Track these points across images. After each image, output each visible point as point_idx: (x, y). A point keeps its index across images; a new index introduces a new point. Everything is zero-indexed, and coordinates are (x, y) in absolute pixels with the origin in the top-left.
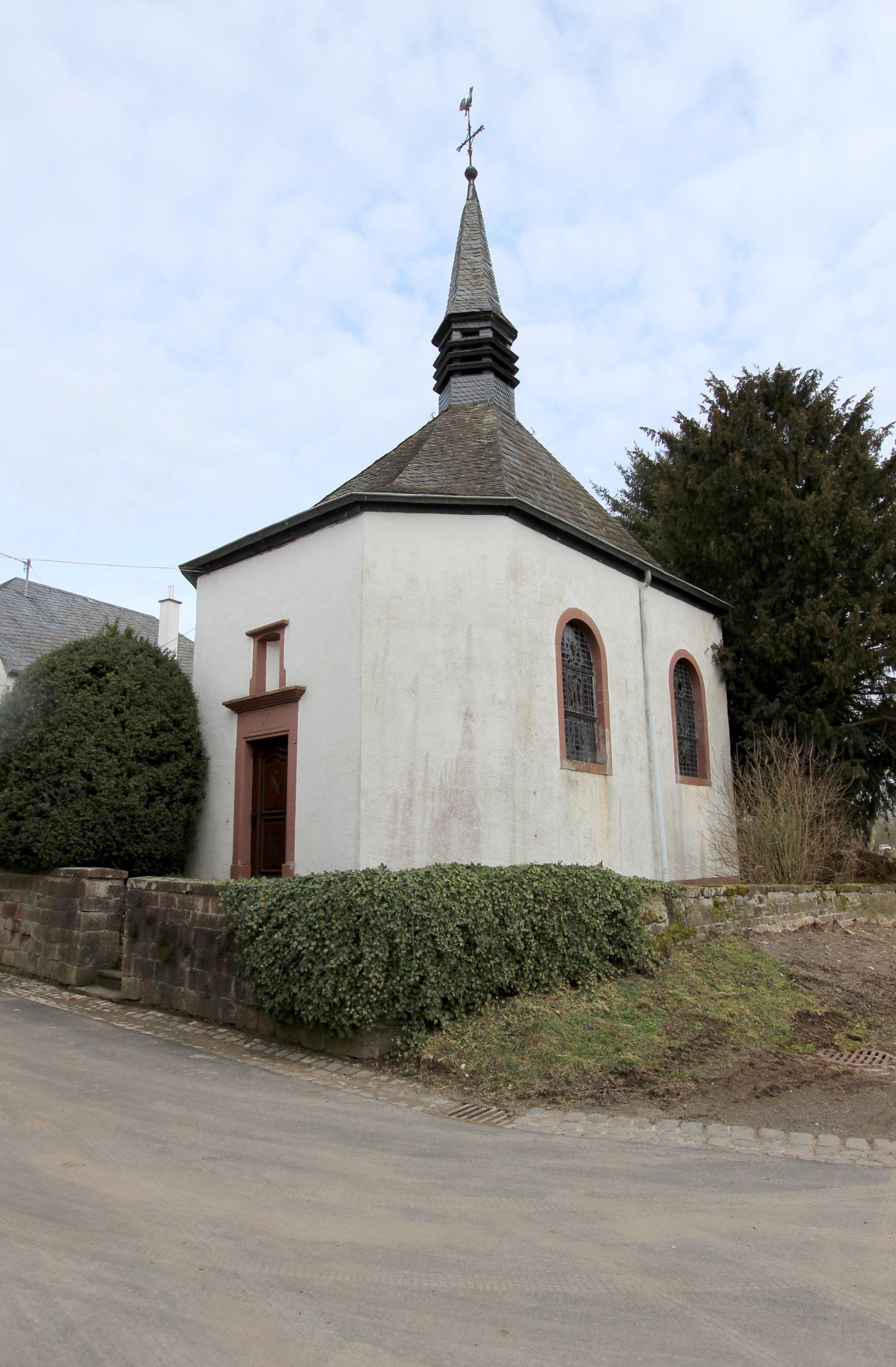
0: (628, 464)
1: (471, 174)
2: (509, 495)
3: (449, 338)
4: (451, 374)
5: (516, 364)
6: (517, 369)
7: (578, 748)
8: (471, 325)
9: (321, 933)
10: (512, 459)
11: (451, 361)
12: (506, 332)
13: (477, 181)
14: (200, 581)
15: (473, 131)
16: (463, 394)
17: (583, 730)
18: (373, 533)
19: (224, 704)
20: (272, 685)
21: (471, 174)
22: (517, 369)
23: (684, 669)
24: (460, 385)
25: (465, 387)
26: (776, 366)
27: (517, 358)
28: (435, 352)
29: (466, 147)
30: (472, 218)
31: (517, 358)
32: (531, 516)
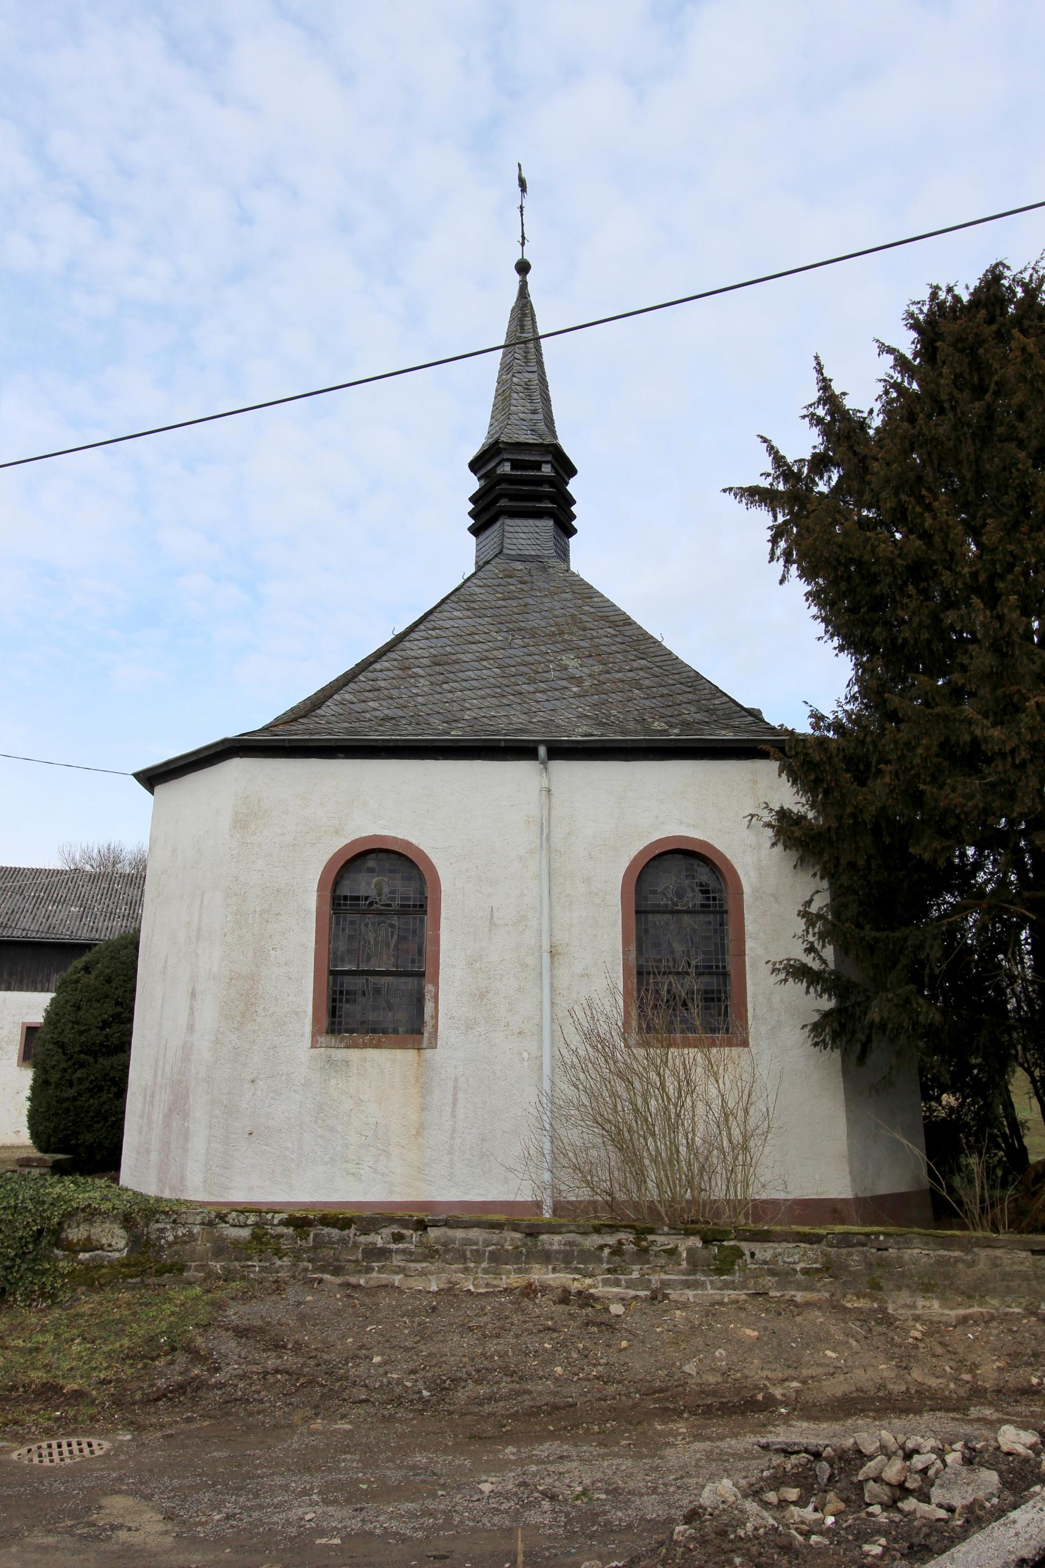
1: (523, 268)
9: (122, 1452)
12: (566, 469)
21: (523, 268)
24: (518, 529)
27: (574, 502)
28: (473, 484)
30: (523, 310)
31: (574, 502)
32: (216, 753)
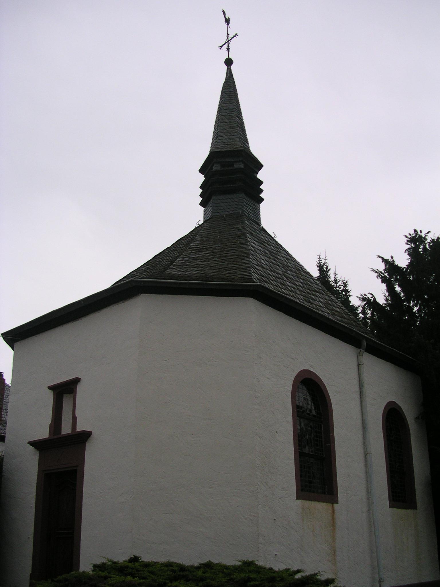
1: (229, 62)
2: (254, 282)
3: (212, 168)
7: (310, 482)
8: (228, 160)
10: (258, 255)
14: (16, 345)
15: (230, 36)
16: (222, 208)
17: (316, 475)
18: (141, 306)
19: (29, 443)
20: (66, 429)
21: (229, 62)
23: (392, 416)
26: (413, 231)
29: (226, 46)
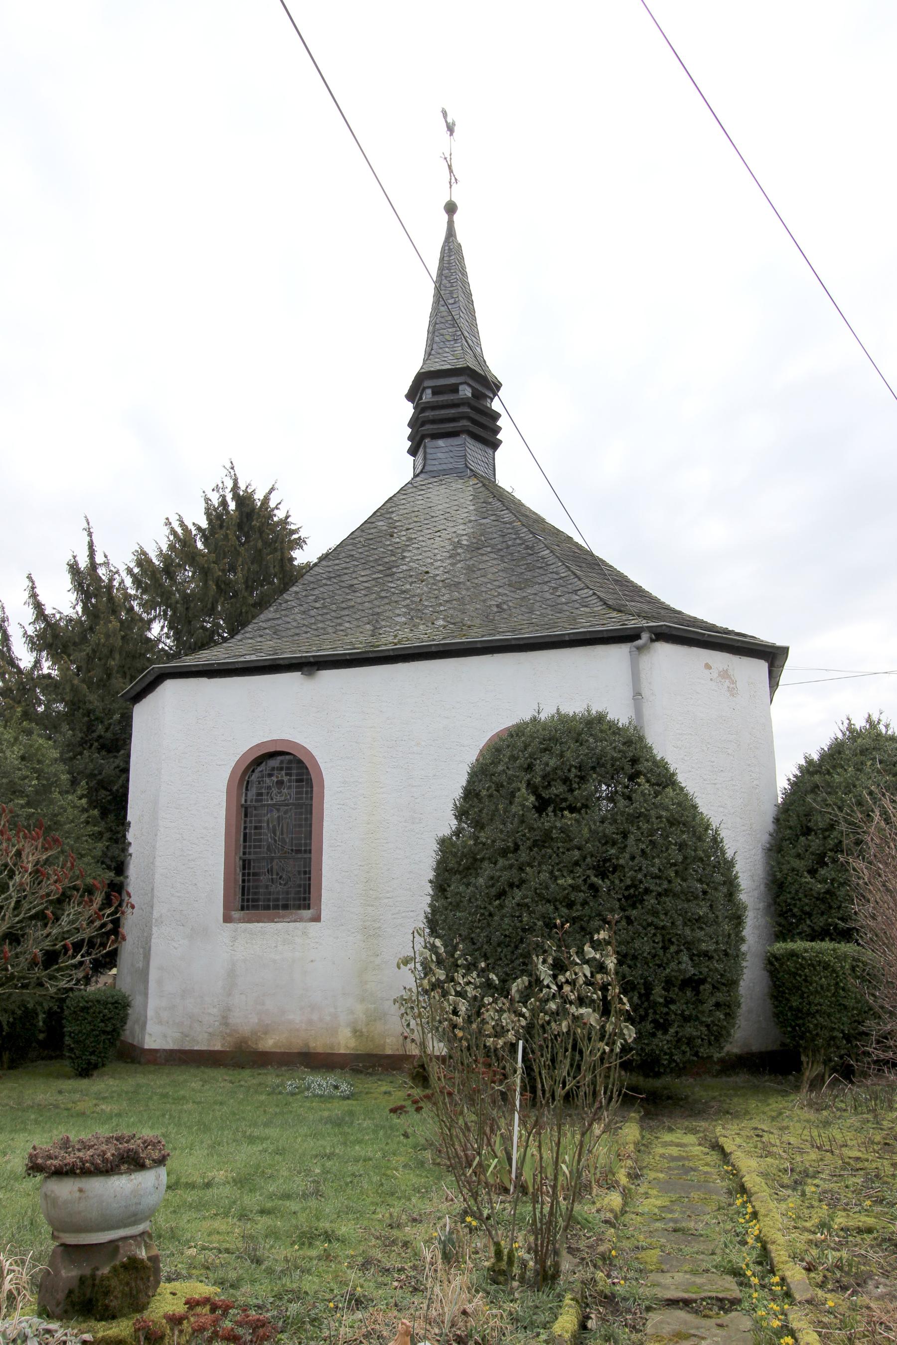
0: (803, 762)
1: (451, 209)
4: (423, 437)
5: (499, 437)
6: (500, 428)
11: (423, 424)
13: (456, 217)
21: (451, 209)
22: (500, 428)
25: (442, 450)
27: (498, 386)
